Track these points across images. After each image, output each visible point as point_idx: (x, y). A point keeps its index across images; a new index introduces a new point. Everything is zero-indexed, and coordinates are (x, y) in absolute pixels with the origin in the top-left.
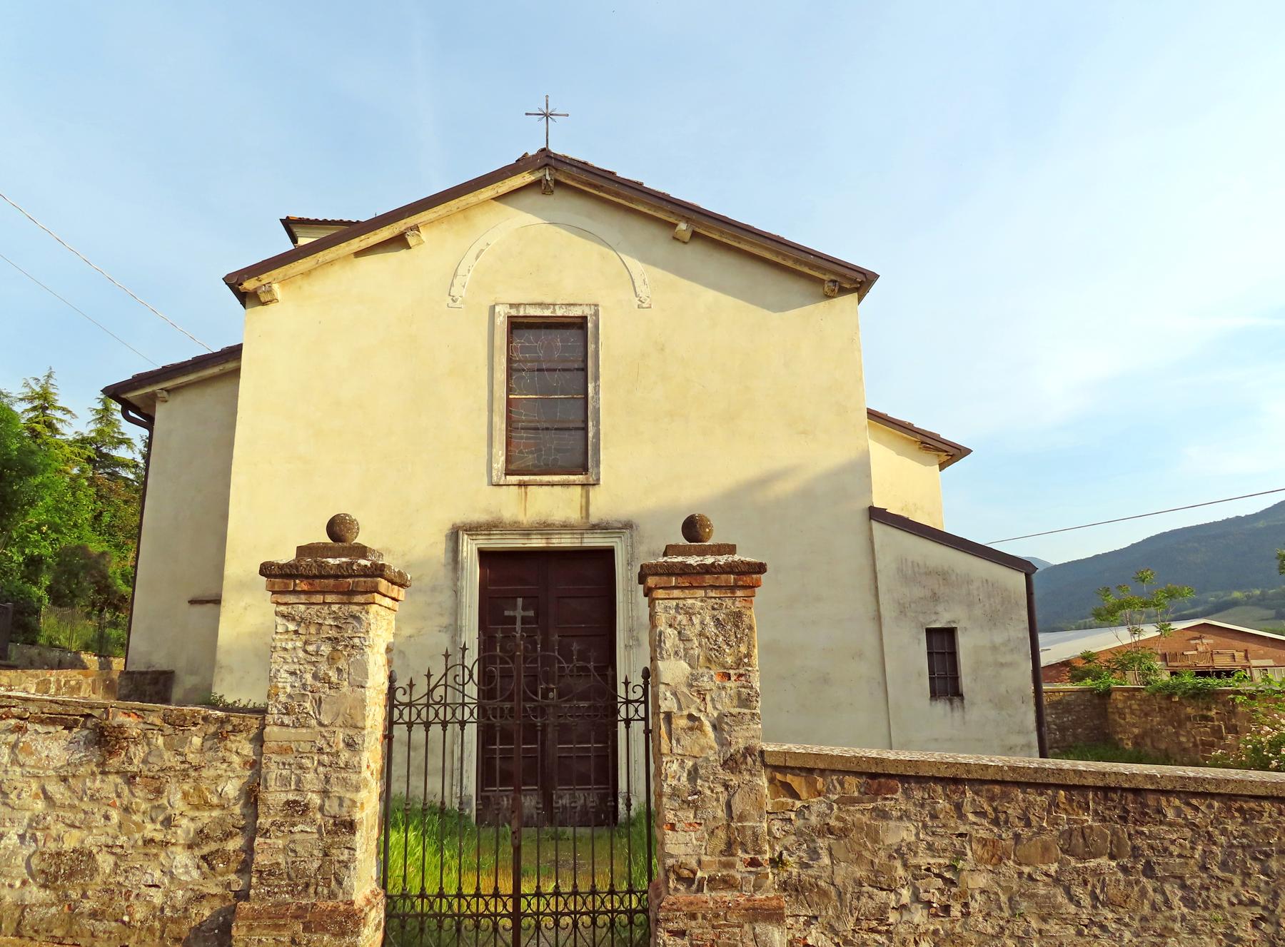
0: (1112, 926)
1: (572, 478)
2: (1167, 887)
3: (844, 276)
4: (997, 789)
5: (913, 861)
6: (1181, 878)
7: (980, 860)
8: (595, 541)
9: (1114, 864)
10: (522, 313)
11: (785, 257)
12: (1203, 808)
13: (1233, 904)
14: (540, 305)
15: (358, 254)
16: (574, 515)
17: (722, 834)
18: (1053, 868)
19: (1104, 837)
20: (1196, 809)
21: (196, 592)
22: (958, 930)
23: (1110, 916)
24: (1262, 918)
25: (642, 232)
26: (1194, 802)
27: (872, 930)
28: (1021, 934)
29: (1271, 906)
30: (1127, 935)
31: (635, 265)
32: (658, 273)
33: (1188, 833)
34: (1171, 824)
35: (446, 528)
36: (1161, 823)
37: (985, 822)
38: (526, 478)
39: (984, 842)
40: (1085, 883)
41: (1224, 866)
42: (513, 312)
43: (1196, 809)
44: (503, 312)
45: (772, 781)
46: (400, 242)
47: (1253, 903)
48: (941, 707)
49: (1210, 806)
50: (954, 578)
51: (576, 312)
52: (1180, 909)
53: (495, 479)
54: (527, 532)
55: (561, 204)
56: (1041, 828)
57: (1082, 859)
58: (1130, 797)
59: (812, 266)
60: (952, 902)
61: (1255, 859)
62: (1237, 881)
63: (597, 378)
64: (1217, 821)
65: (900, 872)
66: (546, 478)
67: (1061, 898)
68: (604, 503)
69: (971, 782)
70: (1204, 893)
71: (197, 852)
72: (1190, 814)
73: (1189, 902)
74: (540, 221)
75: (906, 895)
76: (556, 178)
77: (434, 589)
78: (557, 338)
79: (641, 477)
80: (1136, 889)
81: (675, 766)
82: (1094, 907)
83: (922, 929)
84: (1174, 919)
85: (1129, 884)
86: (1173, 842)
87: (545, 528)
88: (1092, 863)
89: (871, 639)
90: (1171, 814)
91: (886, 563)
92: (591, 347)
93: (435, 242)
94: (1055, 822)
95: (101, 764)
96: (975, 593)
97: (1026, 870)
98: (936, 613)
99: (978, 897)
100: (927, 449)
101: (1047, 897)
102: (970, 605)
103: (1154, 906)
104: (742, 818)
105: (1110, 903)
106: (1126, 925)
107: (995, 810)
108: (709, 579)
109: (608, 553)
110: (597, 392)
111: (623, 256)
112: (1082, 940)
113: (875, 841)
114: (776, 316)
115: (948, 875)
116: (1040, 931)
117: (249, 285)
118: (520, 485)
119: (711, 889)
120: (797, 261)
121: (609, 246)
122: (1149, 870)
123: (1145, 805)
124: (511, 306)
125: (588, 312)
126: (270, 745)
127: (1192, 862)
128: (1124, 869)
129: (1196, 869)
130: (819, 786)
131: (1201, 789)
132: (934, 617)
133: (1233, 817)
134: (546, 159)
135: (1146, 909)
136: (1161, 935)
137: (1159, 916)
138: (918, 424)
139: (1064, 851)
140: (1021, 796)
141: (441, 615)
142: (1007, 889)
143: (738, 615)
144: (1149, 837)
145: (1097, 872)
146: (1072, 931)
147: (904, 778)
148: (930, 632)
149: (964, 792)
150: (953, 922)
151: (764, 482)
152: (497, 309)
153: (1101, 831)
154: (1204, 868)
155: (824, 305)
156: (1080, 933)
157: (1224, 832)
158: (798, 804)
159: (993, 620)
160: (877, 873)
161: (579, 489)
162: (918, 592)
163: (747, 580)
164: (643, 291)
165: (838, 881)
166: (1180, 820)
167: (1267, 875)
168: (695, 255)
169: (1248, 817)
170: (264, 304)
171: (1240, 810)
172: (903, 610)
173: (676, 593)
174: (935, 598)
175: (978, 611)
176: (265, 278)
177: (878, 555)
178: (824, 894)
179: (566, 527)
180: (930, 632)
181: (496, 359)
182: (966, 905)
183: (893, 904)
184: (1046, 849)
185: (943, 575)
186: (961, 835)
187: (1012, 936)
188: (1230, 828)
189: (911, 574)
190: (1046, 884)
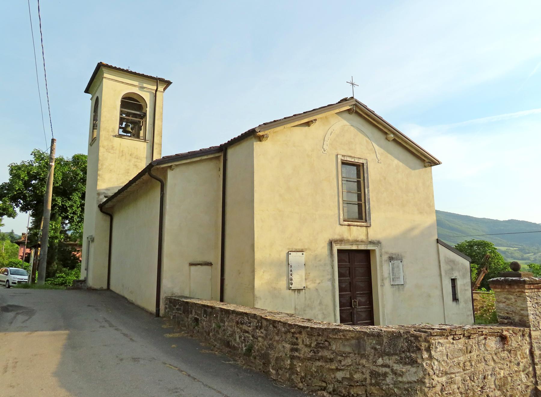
8: (370, 247)
14: (351, 157)
21: (191, 260)
35: (327, 241)
38: (350, 223)
46: (308, 124)
48: (455, 303)
51: (361, 161)
55: (354, 118)
63: (368, 187)
71: (525, 373)
74: (348, 124)
76: (358, 111)
77: (325, 265)
87: (356, 242)
89: (439, 283)
92: (366, 175)
95: (503, 348)
110: (368, 192)
111: (373, 144)
118: (349, 225)
124: (343, 156)
125: (364, 162)
126: (533, 337)
151: (412, 229)
152: (339, 156)
155: (424, 169)
159: (464, 276)
174: (452, 269)
177: (441, 255)
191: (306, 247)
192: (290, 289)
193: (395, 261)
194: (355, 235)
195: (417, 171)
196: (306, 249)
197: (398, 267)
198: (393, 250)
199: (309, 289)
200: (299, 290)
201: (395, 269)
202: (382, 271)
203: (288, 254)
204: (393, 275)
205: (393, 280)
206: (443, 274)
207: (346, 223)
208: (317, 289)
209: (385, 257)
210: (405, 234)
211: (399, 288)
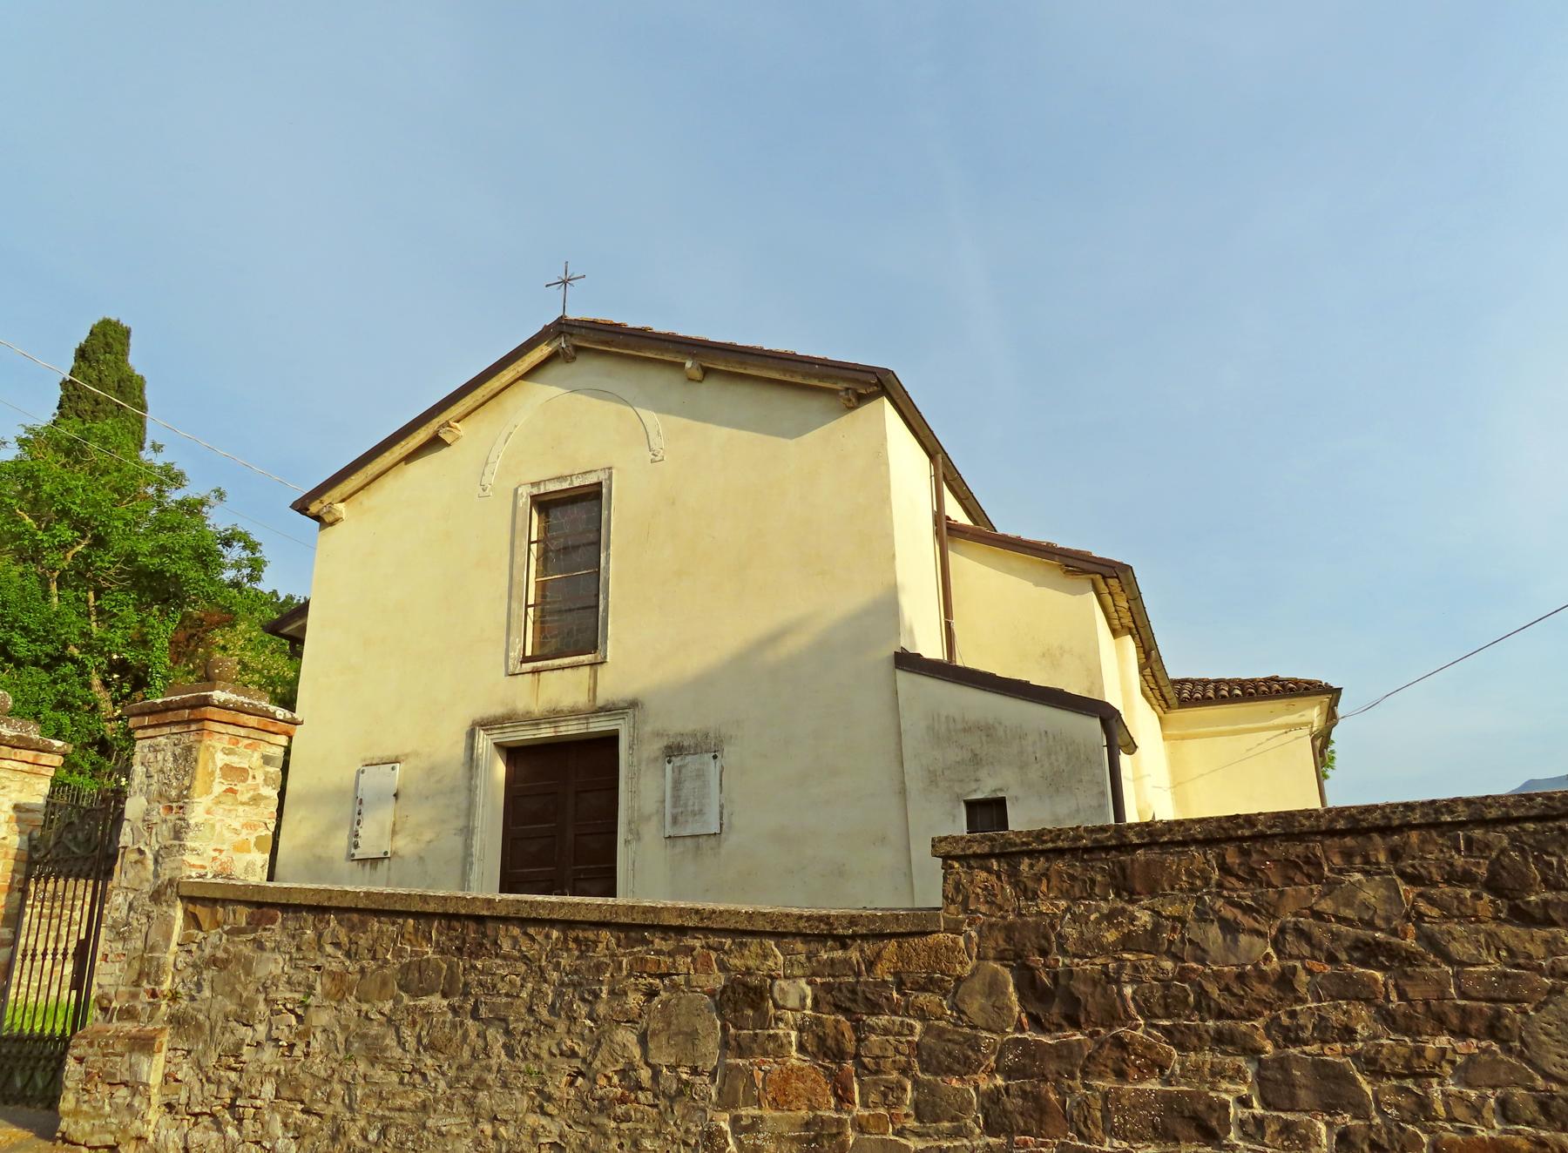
0: (431, 1074)
1: (582, 658)
2: (491, 1032)
3: (857, 381)
4: (355, 917)
5: (272, 996)
6: (505, 1020)
7: (327, 995)
8: (600, 726)
9: (445, 1003)
10: (542, 491)
11: (793, 373)
12: (539, 938)
13: (552, 1055)
15: (409, 458)
16: (580, 698)
17: (136, 965)
18: (387, 1006)
19: (439, 970)
20: (533, 939)
22: (297, 1070)
23: (429, 1062)
24: (580, 1073)
25: (658, 380)
26: (531, 931)
27: (230, 1068)
28: (349, 1079)
29: (589, 1059)
30: (442, 1085)
31: (650, 417)
32: (674, 421)
33: (522, 968)
34: (505, 958)
36: (497, 955)
37: (339, 954)
38: (539, 664)
39: (332, 975)
40: (414, 1023)
41: (552, 1009)
42: (535, 491)
43: (533, 939)
44: (525, 492)
45: (185, 911)
46: (435, 443)
47: (574, 1054)
49: (548, 937)
50: (1001, 732)
51: (591, 479)
52: (499, 1056)
53: (511, 669)
54: (536, 722)
55: (587, 370)
56: (386, 961)
57: (415, 995)
58: (472, 926)
59: (821, 378)
60: (297, 1041)
61: (583, 1000)
62: (561, 1027)
63: (608, 547)
64: (553, 954)
65: (262, 1006)
66: (557, 662)
67: (390, 1041)
68: (615, 681)
69: (338, 910)
70: (525, 1039)
72: (525, 945)
73: (509, 1051)
74: (562, 391)
75: (262, 1029)
76: (578, 343)
77: (453, 790)
78: (576, 511)
79: (654, 645)
80: (460, 1032)
81: (120, 899)
82: (418, 1051)
83: (266, 1069)
84: (489, 1069)
85: (454, 1026)
86: (503, 978)
87: (554, 716)
88: (423, 1002)
90: (506, 946)
91: (914, 722)
93: (470, 436)
94: (399, 954)
96: (1030, 749)
97: (365, 1007)
98: (977, 780)
99: (318, 1035)
100: (1073, 573)
101: (376, 1038)
102: (1023, 766)
103: (474, 1056)
104: (152, 949)
105: (432, 1047)
106: (443, 1074)
107: (350, 942)
108: (170, 716)
109: (611, 740)
110: (608, 562)
112: (401, 1088)
113: (248, 974)
114: (791, 443)
115: (299, 1011)
116: (365, 1077)
117: (314, 508)
118: (535, 672)
119: (119, 1019)
120: (806, 375)
121: (626, 403)
122: (475, 1014)
123: (485, 935)
125: (602, 476)
127: (519, 1002)
128: (455, 1010)
129: (523, 1010)
130: (220, 917)
131: (534, 915)
132: (974, 786)
133: (568, 950)
134: (561, 327)
135: (466, 1054)
136: (473, 1088)
137: (476, 1065)
138: (1061, 543)
139: (401, 987)
140: (376, 926)
141: (457, 817)
142: (345, 1028)
143: (189, 749)
144: (482, 972)
145: (426, 1013)
146: (394, 1078)
147: (285, 907)
148: (971, 806)
149: (328, 923)
150: (294, 1062)
151: (774, 638)
153: (438, 965)
154: (531, 1011)
156: (401, 1082)
157: (557, 967)
158: (201, 935)
160: (243, 1006)
161: (587, 669)
162: (954, 755)
163: (197, 714)
164: (657, 443)
165: (213, 1015)
166: (516, 953)
167: (592, 1020)
168: (709, 391)
169: (585, 946)
170: (332, 524)
171: (576, 940)
172: (933, 778)
173: (150, 732)
174: (976, 760)
175: (1034, 774)
176: (326, 498)
177: (904, 712)
178: (199, 1027)
179: (575, 713)
180: (971, 806)
181: (517, 543)
182: (308, 1044)
183: (248, 1041)
184: (384, 983)
185: (987, 730)
186: (318, 968)
187: (341, 1081)
188: (563, 962)
189: (945, 732)
190: (381, 1024)
191: (407, 750)
192: (351, 857)
193: (689, 758)
194: (562, 690)
195: (809, 437)
196: (407, 755)
197: (700, 775)
198: (682, 724)
199: (401, 857)
200: (375, 861)
201: (688, 786)
202: (641, 790)
203: (471, 735)
204: (675, 806)
205: (675, 821)
206: (914, 785)
207: (528, 666)
208: (421, 858)
209: (655, 747)
210: (743, 663)
211: (698, 847)
